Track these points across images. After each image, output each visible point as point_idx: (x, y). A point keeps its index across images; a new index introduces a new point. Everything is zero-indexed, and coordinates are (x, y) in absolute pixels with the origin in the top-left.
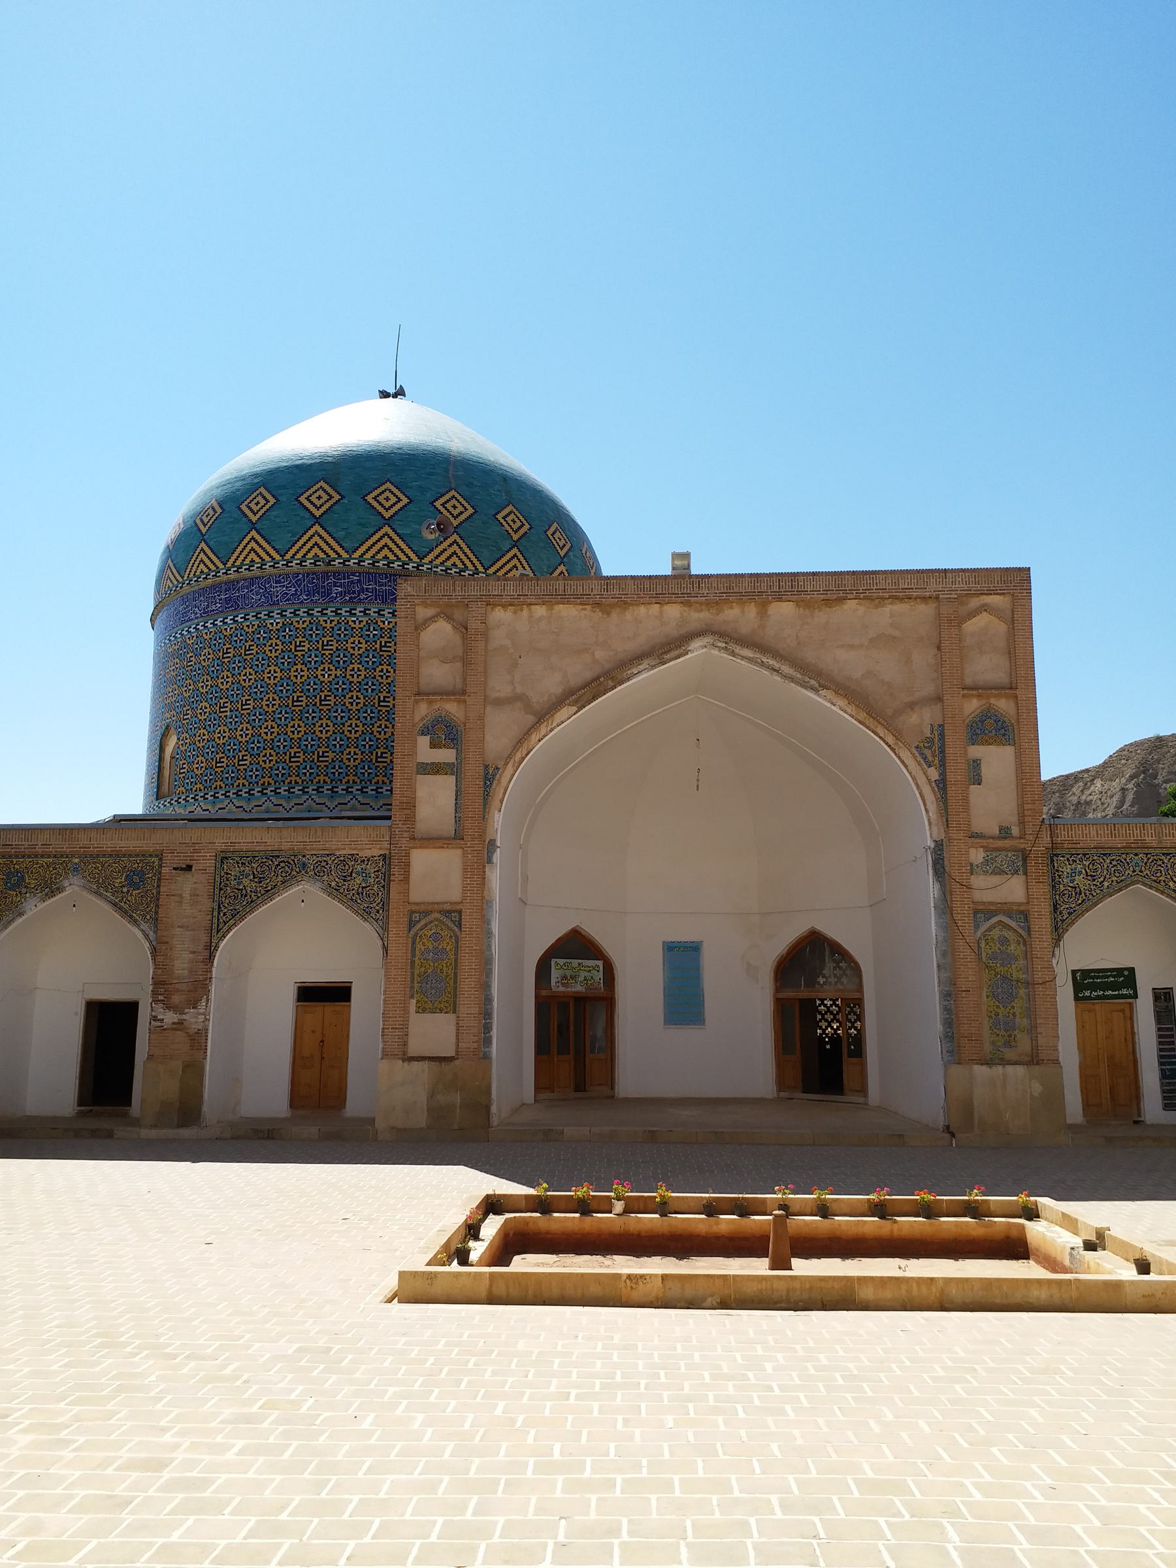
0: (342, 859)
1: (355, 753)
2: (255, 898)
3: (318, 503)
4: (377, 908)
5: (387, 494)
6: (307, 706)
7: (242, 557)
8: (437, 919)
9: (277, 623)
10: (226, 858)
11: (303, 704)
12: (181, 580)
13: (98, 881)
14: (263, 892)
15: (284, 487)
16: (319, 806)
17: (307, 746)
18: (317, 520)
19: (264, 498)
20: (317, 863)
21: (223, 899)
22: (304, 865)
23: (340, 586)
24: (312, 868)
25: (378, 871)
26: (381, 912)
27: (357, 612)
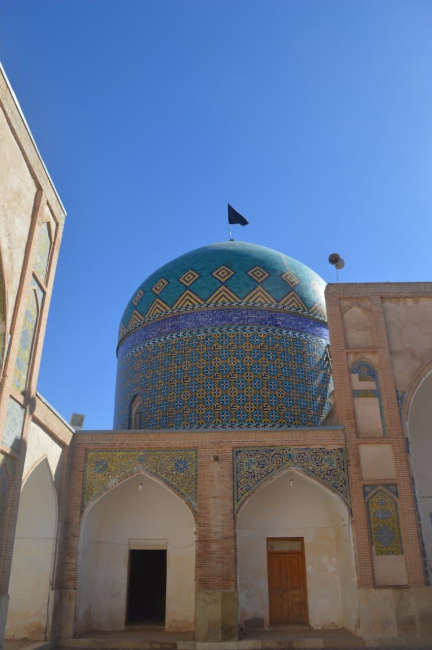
0: (315, 451)
1: (251, 406)
2: (260, 478)
4: (341, 484)
5: (258, 271)
6: (222, 379)
7: (180, 305)
8: (380, 490)
9: (203, 336)
10: (240, 452)
11: (220, 378)
12: (143, 319)
13: (156, 467)
14: (265, 474)
15: (203, 269)
17: (223, 401)
18: (223, 284)
20: (298, 454)
21: (240, 479)
22: (290, 456)
23: (237, 316)
24: (296, 457)
25: (339, 459)
26: (344, 486)
27: (247, 329)
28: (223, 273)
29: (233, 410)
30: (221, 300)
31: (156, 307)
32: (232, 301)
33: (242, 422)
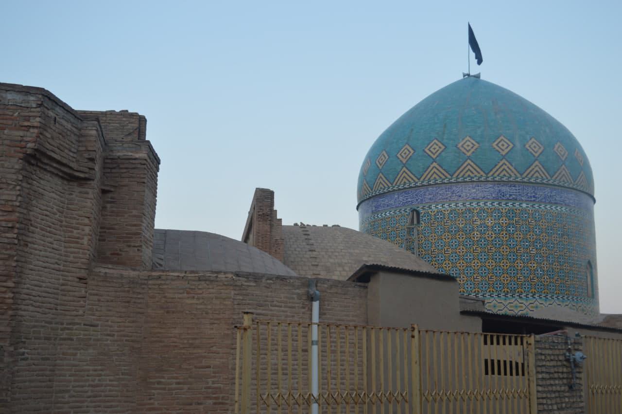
3: (434, 151)
7: (399, 182)
12: (371, 191)
19: (408, 150)
28: (434, 149)
31: (403, 176)
32: (544, 177)
33: (469, 292)
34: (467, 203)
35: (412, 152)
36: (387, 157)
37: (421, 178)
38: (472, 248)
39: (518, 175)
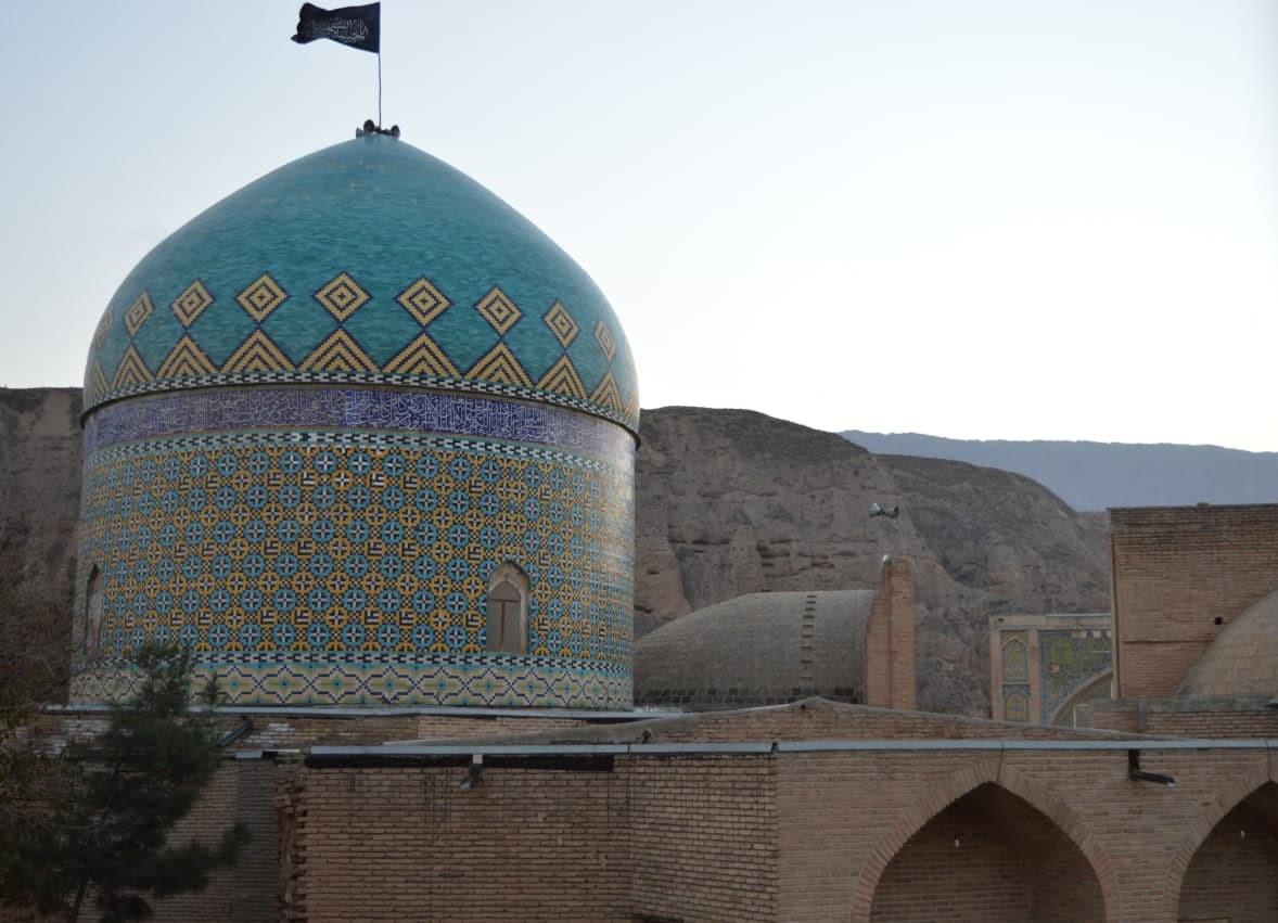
5: (424, 295)
6: (485, 559)
16: (325, 690)
29: (301, 623)
30: (252, 366)
32: (443, 374)
34: (345, 435)
35: (208, 300)
36: (175, 306)
37: (223, 366)
38: (263, 544)
39: (374, 368)
